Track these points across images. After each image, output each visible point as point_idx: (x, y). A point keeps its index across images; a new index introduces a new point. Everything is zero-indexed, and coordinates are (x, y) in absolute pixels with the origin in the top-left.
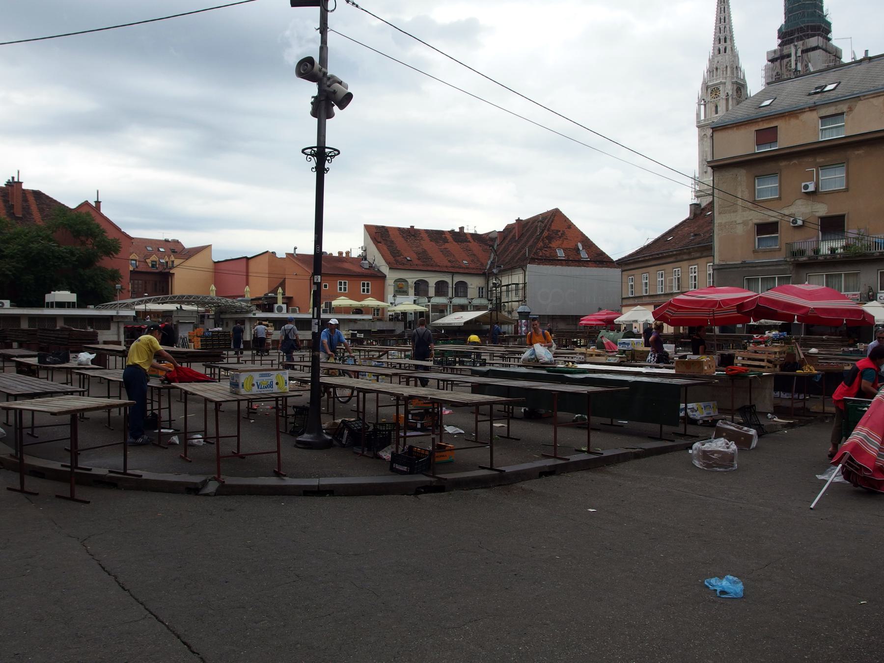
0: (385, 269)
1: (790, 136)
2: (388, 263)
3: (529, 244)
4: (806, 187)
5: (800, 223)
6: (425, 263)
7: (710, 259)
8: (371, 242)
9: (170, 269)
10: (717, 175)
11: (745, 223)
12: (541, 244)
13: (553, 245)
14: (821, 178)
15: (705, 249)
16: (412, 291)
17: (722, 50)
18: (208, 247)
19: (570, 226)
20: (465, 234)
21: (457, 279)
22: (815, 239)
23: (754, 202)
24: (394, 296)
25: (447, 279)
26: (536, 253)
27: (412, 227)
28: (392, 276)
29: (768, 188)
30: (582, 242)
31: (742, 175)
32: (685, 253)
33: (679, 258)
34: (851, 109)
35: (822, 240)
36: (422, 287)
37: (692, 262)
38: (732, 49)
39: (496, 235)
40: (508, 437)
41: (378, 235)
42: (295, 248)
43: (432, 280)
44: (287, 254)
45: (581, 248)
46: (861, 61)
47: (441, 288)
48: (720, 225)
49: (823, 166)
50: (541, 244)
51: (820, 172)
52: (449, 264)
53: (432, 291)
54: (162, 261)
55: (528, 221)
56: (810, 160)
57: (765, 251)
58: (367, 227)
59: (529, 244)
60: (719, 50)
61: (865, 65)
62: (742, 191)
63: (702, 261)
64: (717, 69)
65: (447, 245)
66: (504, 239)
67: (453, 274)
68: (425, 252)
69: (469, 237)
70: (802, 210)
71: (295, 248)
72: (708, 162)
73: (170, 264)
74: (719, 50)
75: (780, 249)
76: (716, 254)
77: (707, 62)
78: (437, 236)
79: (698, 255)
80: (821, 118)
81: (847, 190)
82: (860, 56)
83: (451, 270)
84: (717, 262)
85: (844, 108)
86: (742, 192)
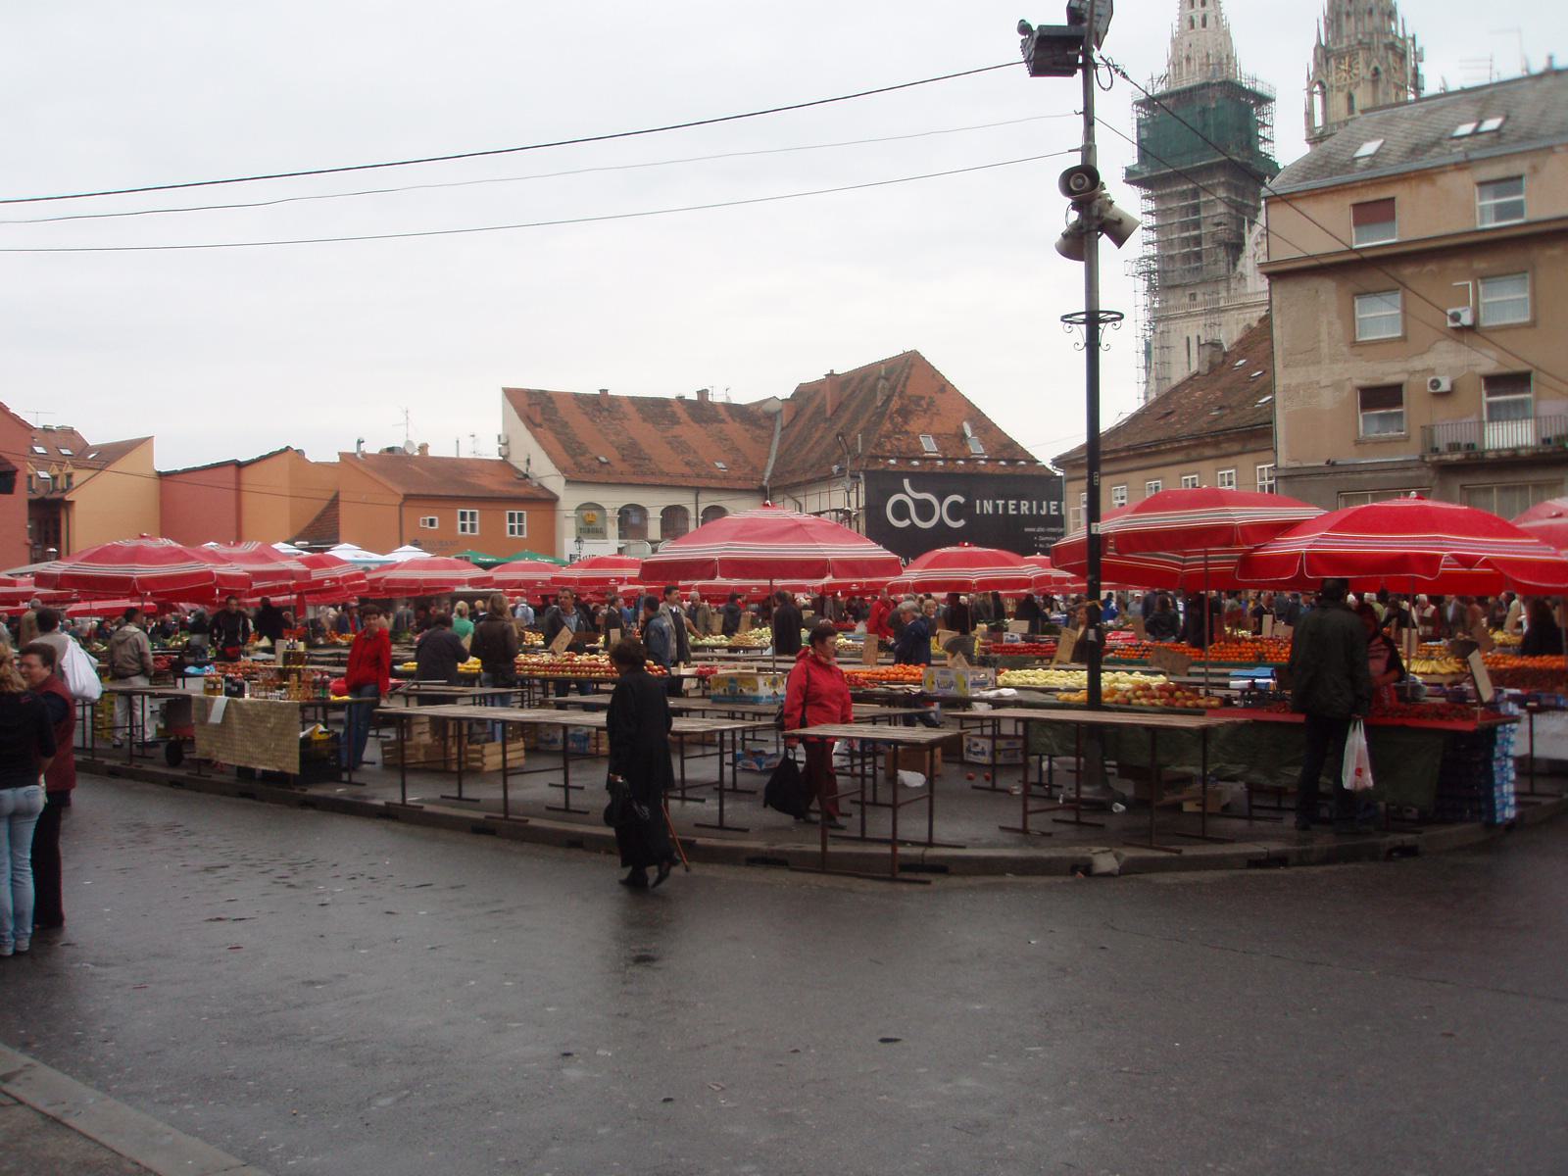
0: (555, 483)
1: (1420, 217)
2: (563, 470)
3: (861, 424)
4: (1456, 317)
5: (1445, 386)
6: (638, 471)
7: (1269, 455)
8: (520, 427)
9: (64, 491)
10: (1278, 287)
11: (1337, 386)
12: (887, 426)
13: (914, 425)
14: (1482, 300)
15: (1257, 435)
16: (613, 529)
17: (1198, 21)
18: (145, 442)
19: (944, 386)
20: (713, 405)
21: (707, 500)
22: (1474, 418)
23: (1354, 344)
24: (579, 540)
25: (685, 500)
26: (879, 445)
27: (604, 392)
28: (570, 500)
29: (1380, 317)
30: (970, 420)
31: (1327, 291)
32: (1207, 444)
33: (1194, 454)
34: (1535, 169)
35: (1491, 420)
36: (635, 519)
37: (1223, 462)
38: (1218, 20)
39: (778, 406)
40: (567, 810)
41: (535, 409)
42: (360, 442)
43: (655, 503)
44: (342, 455)
45: (969, 433)
46: (1540, 76)
47: (673, 520)
48: (1287, 388)
49: (1484, 277)
50: (887, 426)
51: (1481, 288)
52: (687, 470)
53: (654, 530)
54: (43, 474)
55: (849, 378)
56: (1459, 264)
57: (1378, 442)
58: (511, 394)
59: (861, 424)
60: (1192, 21)
61: (1548, 82)
62: (1330, 323)
63: (1245, 461)
64: (1188, 59)
65: (677, 430)
66: (797, 415)
67: (697, 490)
68: (634, 445)
69: (722, 411)
70: (1448, 363)
71: (360, 442)
72: (1261, 265)
73: (61, 483)
74: (1192, 21)
75: (1407, 439)
76: (1281, 447)
77: (1169, 46)
78: (655, 410)
79: (1236, 447)
80: (1481, 184)
81: (1533, 324)
82: (1538, 66)
83: (697, 483)
84: (1282, 462)
85: (1519, 167)
86: (1329, 326)
